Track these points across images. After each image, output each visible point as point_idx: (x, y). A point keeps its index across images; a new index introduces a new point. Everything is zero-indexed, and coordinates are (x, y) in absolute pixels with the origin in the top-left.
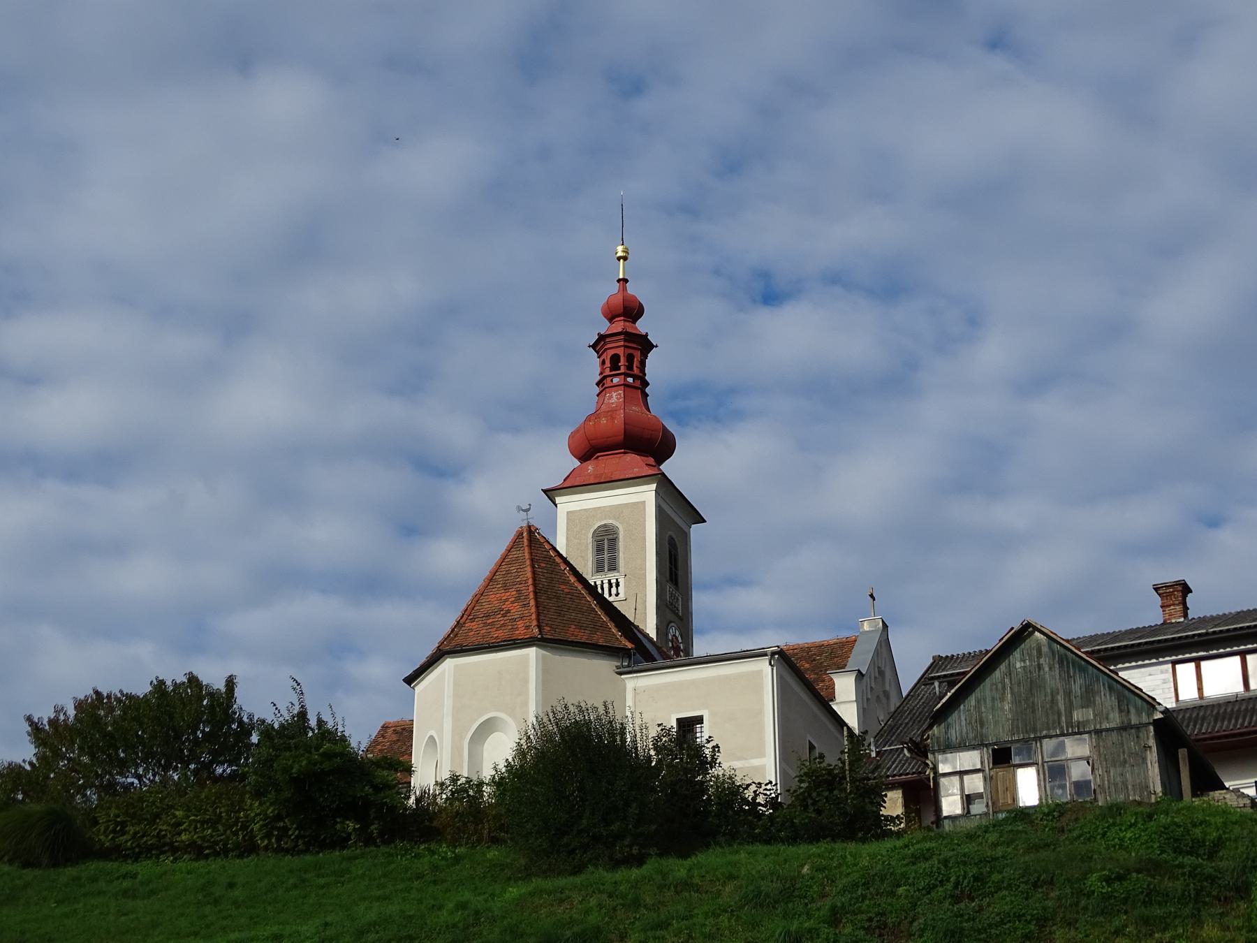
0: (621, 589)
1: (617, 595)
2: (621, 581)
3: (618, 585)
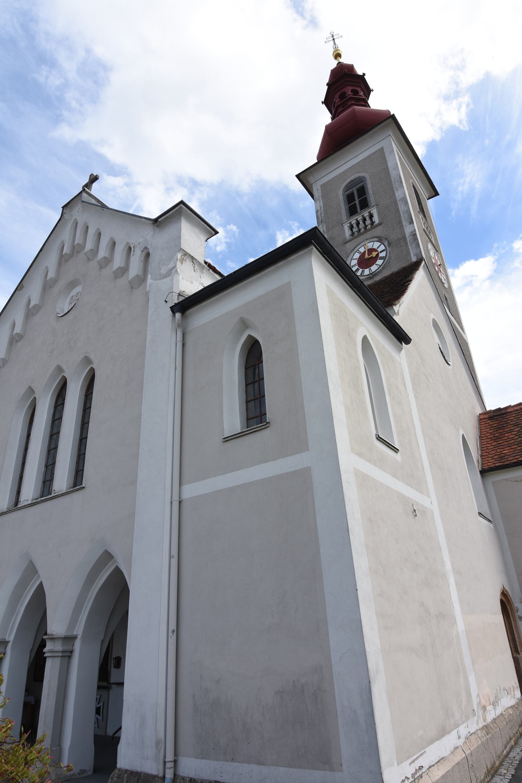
0: (376, 219)
1: (351, 227)
2: (374, 211)
3: (371, 216)
